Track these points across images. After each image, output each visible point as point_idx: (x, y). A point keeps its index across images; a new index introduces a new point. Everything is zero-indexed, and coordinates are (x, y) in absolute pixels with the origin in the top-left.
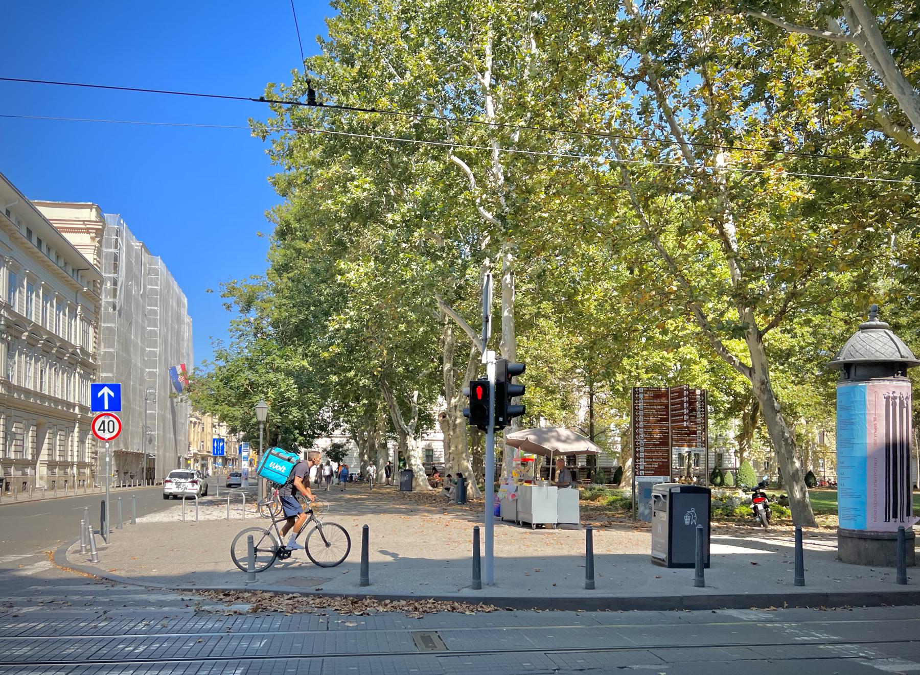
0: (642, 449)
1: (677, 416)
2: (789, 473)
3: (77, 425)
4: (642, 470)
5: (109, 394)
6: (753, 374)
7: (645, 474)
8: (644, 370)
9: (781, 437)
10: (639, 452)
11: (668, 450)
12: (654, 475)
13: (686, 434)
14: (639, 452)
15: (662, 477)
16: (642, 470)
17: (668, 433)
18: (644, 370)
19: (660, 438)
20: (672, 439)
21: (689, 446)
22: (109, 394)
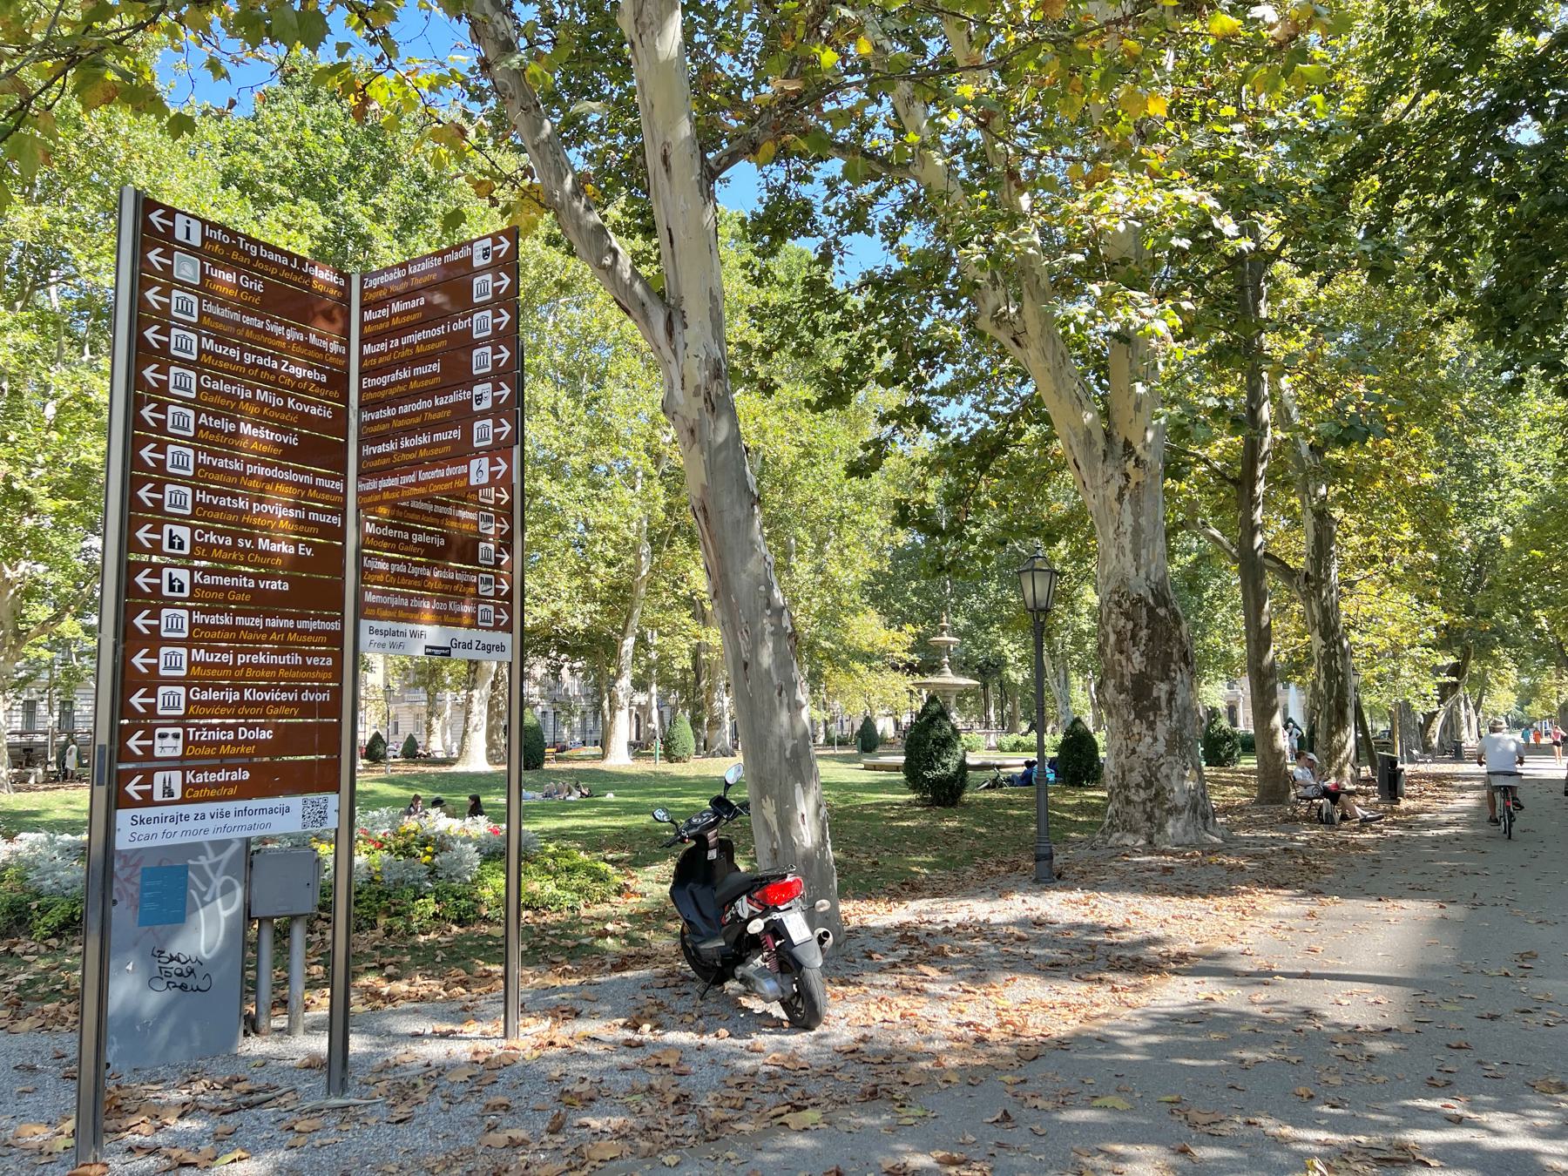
0: (175, 621)
1: (410, 432)
2: (781, 746)
3: (1435, 741)
4: (169, 764)
5: (144, 657)
6: (678, 327)
7: (192, 794)
8: (45, 489)
9: (762, 602)
10: (154, 641)
11: (336, 639)
12: (245, 791)
13: (429, 550)
14: (154, 641)
15: (296, 802)
16: (169, 764)
17: (341, 533)
18: (45, 489)
19: (296, 561)
20: (361, 571)
21: (445, 618)
22: (144, 657)
